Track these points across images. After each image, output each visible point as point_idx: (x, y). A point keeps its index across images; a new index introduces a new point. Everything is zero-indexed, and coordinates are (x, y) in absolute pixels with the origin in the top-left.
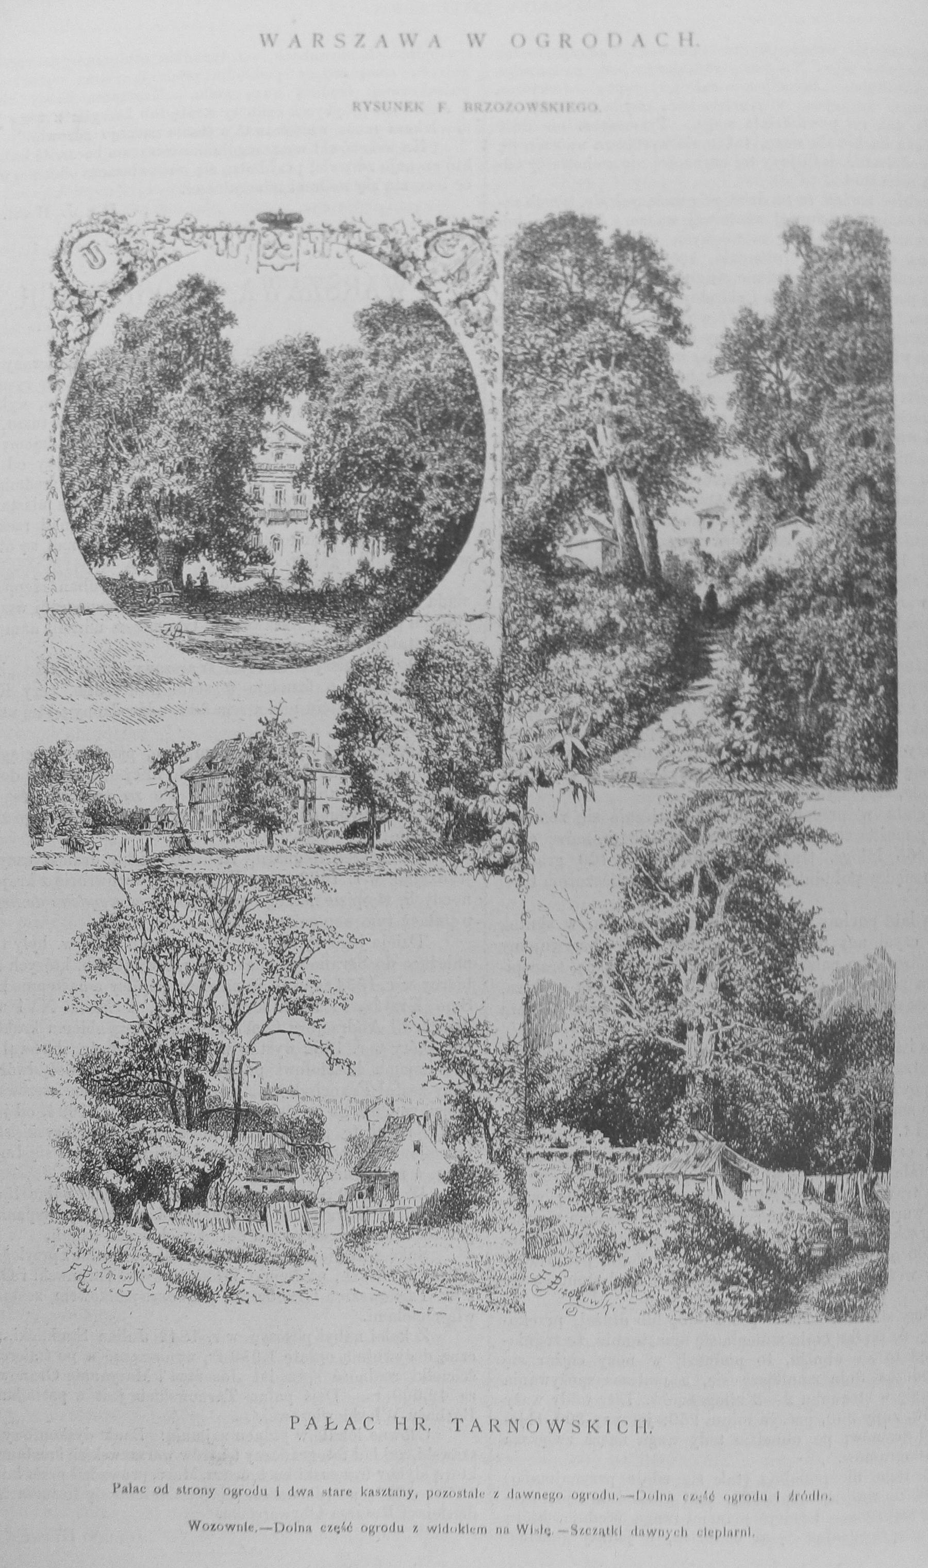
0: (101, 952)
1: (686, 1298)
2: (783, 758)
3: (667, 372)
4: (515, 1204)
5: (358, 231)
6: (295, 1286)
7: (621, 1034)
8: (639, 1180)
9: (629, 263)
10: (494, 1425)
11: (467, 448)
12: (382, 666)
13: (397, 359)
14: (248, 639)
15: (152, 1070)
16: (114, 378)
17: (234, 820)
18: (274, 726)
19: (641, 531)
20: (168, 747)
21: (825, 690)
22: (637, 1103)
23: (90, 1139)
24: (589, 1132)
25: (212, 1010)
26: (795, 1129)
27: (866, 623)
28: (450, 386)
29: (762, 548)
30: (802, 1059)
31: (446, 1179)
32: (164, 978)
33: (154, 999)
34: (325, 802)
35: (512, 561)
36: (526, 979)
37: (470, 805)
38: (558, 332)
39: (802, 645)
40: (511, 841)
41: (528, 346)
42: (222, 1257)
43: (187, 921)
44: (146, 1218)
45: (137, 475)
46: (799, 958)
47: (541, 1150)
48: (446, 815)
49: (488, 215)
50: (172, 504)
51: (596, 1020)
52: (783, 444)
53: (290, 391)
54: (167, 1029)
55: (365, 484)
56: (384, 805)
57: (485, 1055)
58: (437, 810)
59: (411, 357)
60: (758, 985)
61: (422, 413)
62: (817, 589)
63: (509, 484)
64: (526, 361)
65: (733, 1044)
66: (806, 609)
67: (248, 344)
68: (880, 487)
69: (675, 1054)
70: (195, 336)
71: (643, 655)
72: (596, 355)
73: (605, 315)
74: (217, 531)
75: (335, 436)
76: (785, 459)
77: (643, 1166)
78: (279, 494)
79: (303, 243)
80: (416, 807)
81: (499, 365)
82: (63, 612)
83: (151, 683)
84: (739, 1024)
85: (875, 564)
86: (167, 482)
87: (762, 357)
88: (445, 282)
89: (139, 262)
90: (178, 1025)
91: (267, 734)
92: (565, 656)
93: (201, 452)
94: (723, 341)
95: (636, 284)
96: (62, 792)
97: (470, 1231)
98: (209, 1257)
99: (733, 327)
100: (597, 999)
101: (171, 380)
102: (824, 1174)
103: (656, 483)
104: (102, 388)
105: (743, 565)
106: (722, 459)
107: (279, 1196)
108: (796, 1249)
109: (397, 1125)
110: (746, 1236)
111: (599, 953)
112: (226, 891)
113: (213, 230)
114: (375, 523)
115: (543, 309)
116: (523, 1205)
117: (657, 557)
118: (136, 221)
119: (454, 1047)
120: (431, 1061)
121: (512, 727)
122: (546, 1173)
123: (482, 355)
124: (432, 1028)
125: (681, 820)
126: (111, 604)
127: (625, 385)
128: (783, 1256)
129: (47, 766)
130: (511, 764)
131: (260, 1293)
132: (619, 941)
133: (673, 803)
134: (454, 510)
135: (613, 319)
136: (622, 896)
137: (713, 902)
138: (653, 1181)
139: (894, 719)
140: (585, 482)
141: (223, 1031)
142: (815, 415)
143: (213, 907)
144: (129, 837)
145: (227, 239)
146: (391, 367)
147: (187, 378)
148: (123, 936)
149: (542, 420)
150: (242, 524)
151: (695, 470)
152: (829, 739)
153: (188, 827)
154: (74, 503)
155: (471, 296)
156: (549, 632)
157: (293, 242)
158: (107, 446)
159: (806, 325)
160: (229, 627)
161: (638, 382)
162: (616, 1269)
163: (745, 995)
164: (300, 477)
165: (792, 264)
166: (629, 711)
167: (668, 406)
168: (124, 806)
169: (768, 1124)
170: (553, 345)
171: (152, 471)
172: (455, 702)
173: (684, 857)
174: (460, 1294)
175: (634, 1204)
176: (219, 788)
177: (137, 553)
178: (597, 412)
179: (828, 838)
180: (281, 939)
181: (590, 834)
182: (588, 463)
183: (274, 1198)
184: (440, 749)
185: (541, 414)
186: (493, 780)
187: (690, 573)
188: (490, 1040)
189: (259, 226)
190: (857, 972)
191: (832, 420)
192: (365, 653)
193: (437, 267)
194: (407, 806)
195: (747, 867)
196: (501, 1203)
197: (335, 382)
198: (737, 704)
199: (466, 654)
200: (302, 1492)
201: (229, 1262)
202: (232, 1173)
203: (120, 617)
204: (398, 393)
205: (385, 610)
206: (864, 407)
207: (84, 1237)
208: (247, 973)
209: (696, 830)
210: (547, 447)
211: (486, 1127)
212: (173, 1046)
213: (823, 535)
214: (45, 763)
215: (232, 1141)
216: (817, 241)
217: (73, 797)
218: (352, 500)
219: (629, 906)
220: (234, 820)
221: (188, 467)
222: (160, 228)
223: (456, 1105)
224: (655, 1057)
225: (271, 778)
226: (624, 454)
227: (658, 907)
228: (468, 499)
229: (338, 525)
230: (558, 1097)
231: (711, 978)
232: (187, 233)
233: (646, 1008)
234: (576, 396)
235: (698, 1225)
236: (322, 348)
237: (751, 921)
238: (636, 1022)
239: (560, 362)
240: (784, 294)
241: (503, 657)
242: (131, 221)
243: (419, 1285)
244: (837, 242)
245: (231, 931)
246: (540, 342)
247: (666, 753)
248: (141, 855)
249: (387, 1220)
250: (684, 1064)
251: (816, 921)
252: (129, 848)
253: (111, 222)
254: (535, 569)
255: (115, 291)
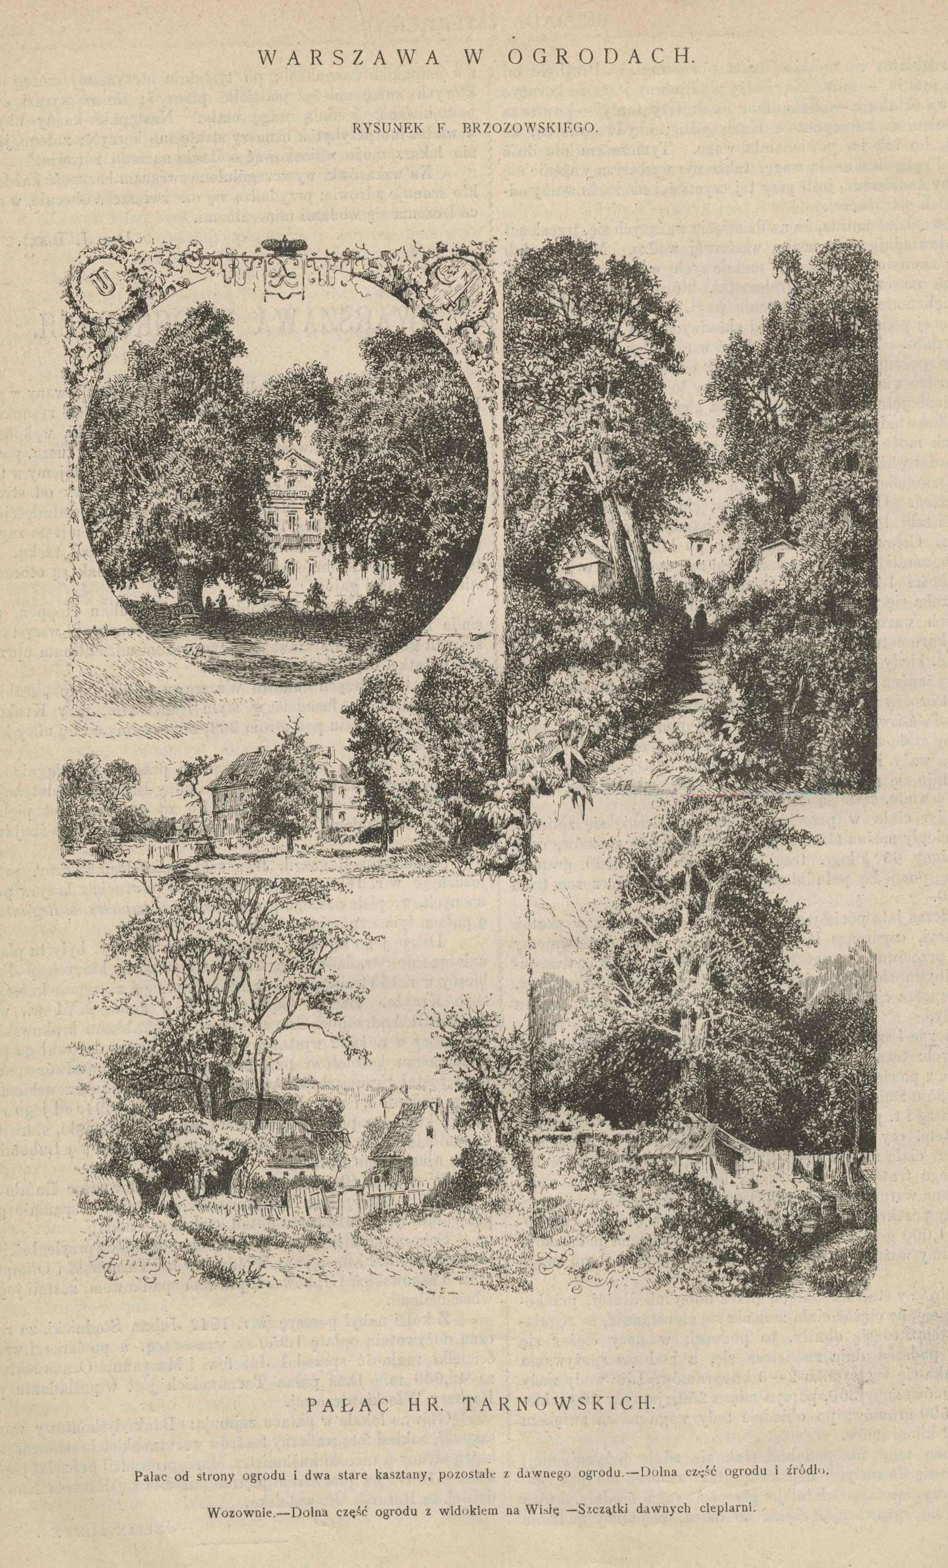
0: (130, 953)
1: (684, 1275)
2: (768, 767)
3: (660, 399)
4: (523, 1185)
7: (620, 1023)
8: (639, 1161)
9: (624, 290)
10: (504, 1404)
11: (470, 474)
12: (394, 683)
13: (402, 387)
14: (266, 658)
15: (179, 1064)
16: (129, 405)
17: (256, 828)
18: (292, 740)
19: (635, 554)
21: (808, 705)
22: (635, 1087)
23: (118, 1131)
24: (591, 1116)
25: (236, 1005)
26: (782, 1112)
27: (847, 640)
28: (453, 414)
29: (749, 571)
31: (457, 1162)
32: (190, 975)
33: (181, 997)
34: (342, 810)
35: (514, 583)
36: (530, 972)
37: (478, 812)
38: (555, 359)
39: (787, 662)
40: (515, 844)
41: (527, 373)
42: (245, 1241)
43: (211, 922)
44: (172, 1205)
45: (156, 501)
46: (785, 951)
47: (546, 1133)
48: (455, 820)
49: (486, 240)
50: (191, 531)
51: (596, 1010)
52: (770, 469)
53: (300, 419)
54: (193, 1024)
56: (397, 811)
57: (493, 1044)
58: (446, 815)
59: (415, 385)
60: (747, 977)
61: (427, 441)
62: (801, 607)
63: (510, 509)
64: (525, 389)
65: (724, 1031)
66: (790, 628)
67: (260, 370)
68: (863, 511)
69: (671, 1041)
70: (206, 364)
71: (637, 671)
72: (592, 382)
73: (601, 342)
74: (235, 556)
75: (344, 462)
76: (771, 484)
77: (642, 1147)
78: (292, 520)
79: (308, 270)
81: (499, 392)
82: (88, 634)
84: (729, 1012)
85: (856, 584)
86: (185, 508)
87: (751, 384)
88: (446, 309)
89: (148, 289)
90: (204, 1021)
91: (285, 747)
92: (564, 674)
93: (216, 480)
94: (714, 368)
95: (630, 311)
96: (90, 803)
97: (480, 1211)
98: (233, 1242)
100: (597, 990)
101: (185, 408)
102: (811, 1153)
104: (118, 415)
105: (731, 586)
106: (712, 484)
107: (301, 1181)
108: (787, 1225)
109: (410, 1111)
110: (739, 1213)
111: (599, 948)
112: (249, 894)
113: (220, 257)
114: (384, 548)
115: (541, 337)
116: (530, 1187)
117: (650, 579)
118: (144, 247)
119: (465, 1038)
120: (442, 1050)
121: (515, 738)
122: (550, 1155)
123: (484, 380)
124: (444, 1019)
125: (674, 824)
126: (135, 626)
127: (620, 411)
128: (776, 1233)
129: (77, 779)
130: (514, 773)
131: (280, 1276)
132: (616, 936)
134: (458, 535)
135: (609, 346)
136: (619, 895)
137: (704, 899)
138: (651, 1161)
139: (873, 729)
140: (581, 507)
142: (801, 441)
143: (237, 909)
144: (156, 845)
145: (234, 267)
146: (396, 395)
147: (201, 406)
148: (151, 938)
149: (541, 447)
150: (258, 549)
151: (686, 495)
152: (812, 748)
153: (212, 834)
154: (95, 528)
155: (472, 324)
156: (550, 649)
157: (298, 270)
158: (125, 472)
159: (794, 352)
160: (247, 647)
161: (633, 409)
162: (618, 1247)
163: (735, 985)
164: (312, 504)
165: (780, 291)
166: (625, 724)
167: (661, 433)
168: (151, 815)
169: (758, 1107)
170: (551, 372)
172: (461, 716)
173: (676, 857)
174: (470, 1274)
175: (634, 1183)
177: (158, 577)
178: (593, 438)
179: (811, 838)
180: (301, 937)
181: (588, 840)
182: (585, 488)
183: (294, 1184)
185: (540, 441)
186: (498, 788)
187: (681, 593)
188: (497, 1030)
189: (264, 252)
190: (840, 964)
192: (378, 670)
193: (439, 295)
194: (418, 813)
195: (734, 867)
196: (509, 1185)
197: (343, 410)
198: (725, 716)
199: (472, 671)
200: (318, 1476)
201: (252, 1247)
202: (254, 1160)
203: (143, 640)
204: (403, 421)
205: (395, 630)
206: (848, 432)
207: (112, 1226)
208: (268, 970)
210: (546, 473)
211: (495, 1113)
212: (199, 1041)
213: (807, 557)
214: (73, 775)
215: (255, 1130)
216: (806, 265)
217: (101, 807)
218: (362, 526)
219: (625, 903)
220: (256, 828)
221: (204, 494)
222: (167, 254)
223: (467, 1092)
224: (652, 1044)
225: (290, 789)
226: (619, 479)
228: (471, 524)
229: (349, 549)
230: (562, 1083)
231: (703, 970)
232: (194, 260)
233: (643, 998)
234: (573, 423)
235: (694, 1203)
236: (330, 377)
237: (740, 916)
238: (633, 1011)
239: (558, 389)
240: (772, 322)
241: (506, 673)
243: (432, 1265)
244: (826, 267)
245: (254, 931)
246: (539, 369)
248: (168, 861)
249: (401, 1203)
250: (678, 1050)
251: (801, 916)
252: (156, 854)
253: (119, 248)
254: (535, 591)
255: (125, 319)
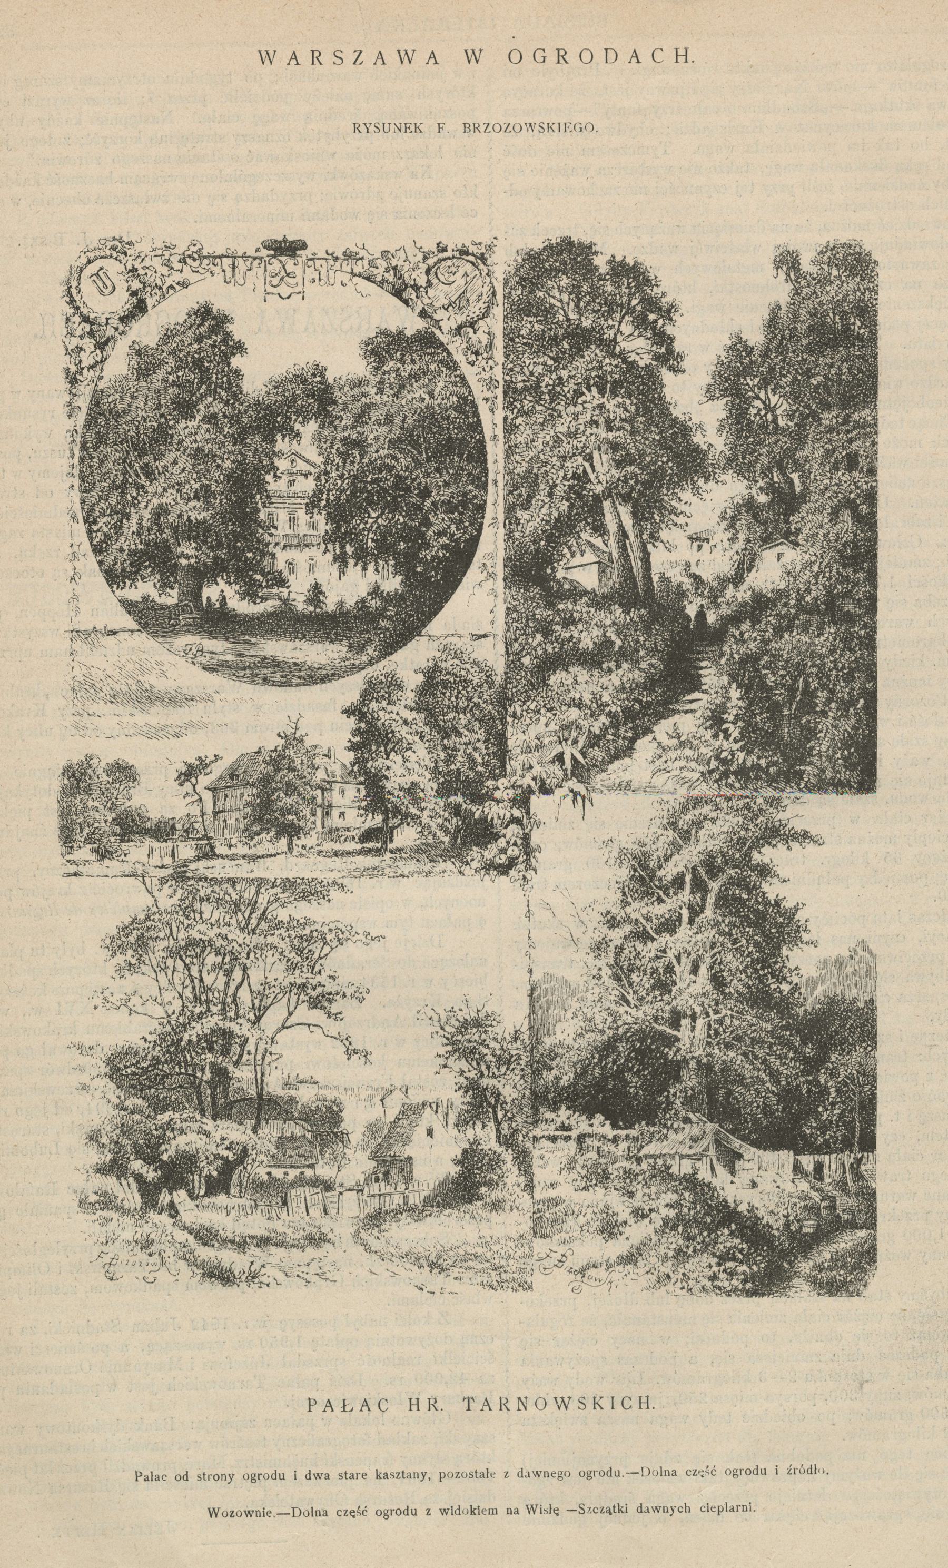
0: (130, 953)
1: (684, 1274)
2: (768, 767)
3: (660, 399)
4: (523, 1185)
5: (362, 258)
6: (314, 1268)
7: (620, 1023)
8: (639, 1161)
9: (624, 290)
11: (470, 474)
12: (394, 683)
13: (402, 387)
14: (265, 658)
15: (179, 1064)
16: (129, 405)
17: (256, 828)
18: (292, 740)
19: (635, 554)
20: (192, 761)
21: (808, 705)
22: (636, 1087)
23: (118, 1131)
24: (591, 1116)
25: (236, 1005)
26: (782, 1112)
27: (847, 640)
28: (453, 414)
29: (749, 570)
30: (789, 1045)
31: (457, 1162)
32: (190, 976)
33: (181, 996)
34: (342, 810)
35: (514, 583)
36: (530, 972)
38: (555, 359)
39: (787, 662)
40: (515, 844)
41: (527, 373)
42: (245, 1241)
43: (211, 922)
44: (172, 1205)
45: (156, 501)
46: (785, 951)
47: (546, 1133)
48: (455, 820)
49: (486, 239)
50: (191, 530)
51: (596, 1010)
52: (770, 469)
53: (300, 419)
54: (193, 1024)
55: (374, 510)
56: (397, 811)
57: (493, 1044)
58: (446, 815)
59: (415, 385)
60: (747, 976)
62: (801, 607)
63: (510, 509)
64: (525, 389)
65: (724, 1031)
66: (790, 628)
67: (260, 370)
68: (863, 511)
69: (671, 1041)
71: (637, 671)
72: (592, 382)
73: (601, 342)
74: (234, 556)
76: (771, 484)
77: (642, 1147)
78: (292, 520)
80: (426, 813)
81: (499, 392)
82: (88, 634)
83: (174, 700)
84: (729, 1012)
85: (856, 584)
86: (185, 508)
87: (751, 383)
88: (446, 309)
89: (148, 289)
90: (204, 1021)
91: (285, 747)
92: (564, 673)
93: (216, 479)
95: (630, 311)
96: (90, 803)
97: (480, 1211)
98: (233, 1242)
99: (723, 354)
100: (597, 990)
101: (185, 408)
103: (649, 507)
104: (118, 415)
105: (731, 586)
106: (712, 484)
107: (301, 1182)
108: (787, 1225)
109: (410, 1111)
110: (739, 1213)
111: (599, 948)
112: (249, 894)
113: (220, 257)
114: (384, 548)
116: (530, 1187)
117: (650, 579)
119: (465, 1038)
120: (442, 1050)
121: (515, 739)
123: (484, 380)
124: (443, 1019)
125: (673, 824)
126: (135, 626)
127: (619, 411)
128: (776, 1233)
129: (77, 779)
130: (514, 773)
131: (280, 1276)
132: (617, 936)
133: (666, 807)
134: (458, 535)
135: (609, 346)
137: (704, 899)
138: (651, 1161)
139: (873, 729)
141: (247, 1025)
142: (801, 441)
143: (237, 909)
144: (156, 845)
145: (234, 267)
146: (396, 396)
147: (201, 406)
148: (151, 938)
149: (541, 447)
150: (258, 549)
151: (686, 495)
152: (812, 748)
153: (212, 834)
154: (95, 528)
155: (472, 324)
156: (550, 650)
157: (298, 270)
158: (125, 472)
159: (794, 352)
160: (247, 647)
161: (633, 409)
162: (618, 1247)
163: (735, 985)
164: (312, 504)
165: (780, 291)
166: (625, 724)
167: (661, 433)
168: (151, 815)
169: (758, 1106)
170: (551, 372)
171: (167, 499)
172: (461, 716)
173: (676, 857)
174: (470, 1274)
175: (634, 1183)
176: (241, 799)
177: (158, 576)
178: (593, 438)
180: (301, 937)
181: (588, 840)
182: (585, 489)
183: (294, 1184)
184: (449, 759)
185: (540, 441)
187: (681, 593)
188: (497, 1030)
189: (264, 252)
190: (840, 964)
191: (817, 445)
192: (378, 670)
193: (439, 295)
194: (418, 813)
196: (509, 1185)
197: (343, 410)
198: (725, 716)
199: (472, 671)
200: (318, 1476)
202: (254, 1160)
203: (143, 640)
204: (403, 421)
205: (395, 630)
206: (848, 432)
207: (113, 1225)
208: (269, 970)
209: (687, 832)
210: (546, 473)
211: (495, 1113)
212: (199, 1041)
213: (807, 557)
214: (73, 775)
215: (255, 1130)
216: (806, 265)
217: (101, 807)
218: (362, 526)
219: (625, 903)
221: (204, 494)
222: (167, 254)
223: (467, 1092)
224: (652, 1044)
225: (290, 789)
226: (619, 479)
227: (652, 903)
229: (349, 549)
230: (562, 1083)
231: (703, 970)
232: (194, 260)
233: (643, 998)
235: (694, 1203)
236: (330, 377)
237: (740, 916)
238: (633, 1011)
239: (558, 389)
240: (772, 322)
241: (506, 673)
242: (138, 247)
244: (826, 267)
245: (254, 931)
246: (539, 369)
247: (657, 763)
248: (168, 861)
249: (401, 1203)
250: (678, 1050)
251: (800, 916)
252: (156, 854)
253: (119, 248)
254: (535, 591)
255: (125, 319)
